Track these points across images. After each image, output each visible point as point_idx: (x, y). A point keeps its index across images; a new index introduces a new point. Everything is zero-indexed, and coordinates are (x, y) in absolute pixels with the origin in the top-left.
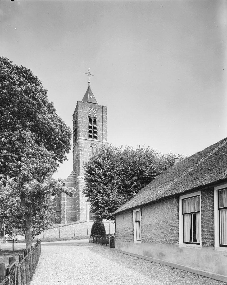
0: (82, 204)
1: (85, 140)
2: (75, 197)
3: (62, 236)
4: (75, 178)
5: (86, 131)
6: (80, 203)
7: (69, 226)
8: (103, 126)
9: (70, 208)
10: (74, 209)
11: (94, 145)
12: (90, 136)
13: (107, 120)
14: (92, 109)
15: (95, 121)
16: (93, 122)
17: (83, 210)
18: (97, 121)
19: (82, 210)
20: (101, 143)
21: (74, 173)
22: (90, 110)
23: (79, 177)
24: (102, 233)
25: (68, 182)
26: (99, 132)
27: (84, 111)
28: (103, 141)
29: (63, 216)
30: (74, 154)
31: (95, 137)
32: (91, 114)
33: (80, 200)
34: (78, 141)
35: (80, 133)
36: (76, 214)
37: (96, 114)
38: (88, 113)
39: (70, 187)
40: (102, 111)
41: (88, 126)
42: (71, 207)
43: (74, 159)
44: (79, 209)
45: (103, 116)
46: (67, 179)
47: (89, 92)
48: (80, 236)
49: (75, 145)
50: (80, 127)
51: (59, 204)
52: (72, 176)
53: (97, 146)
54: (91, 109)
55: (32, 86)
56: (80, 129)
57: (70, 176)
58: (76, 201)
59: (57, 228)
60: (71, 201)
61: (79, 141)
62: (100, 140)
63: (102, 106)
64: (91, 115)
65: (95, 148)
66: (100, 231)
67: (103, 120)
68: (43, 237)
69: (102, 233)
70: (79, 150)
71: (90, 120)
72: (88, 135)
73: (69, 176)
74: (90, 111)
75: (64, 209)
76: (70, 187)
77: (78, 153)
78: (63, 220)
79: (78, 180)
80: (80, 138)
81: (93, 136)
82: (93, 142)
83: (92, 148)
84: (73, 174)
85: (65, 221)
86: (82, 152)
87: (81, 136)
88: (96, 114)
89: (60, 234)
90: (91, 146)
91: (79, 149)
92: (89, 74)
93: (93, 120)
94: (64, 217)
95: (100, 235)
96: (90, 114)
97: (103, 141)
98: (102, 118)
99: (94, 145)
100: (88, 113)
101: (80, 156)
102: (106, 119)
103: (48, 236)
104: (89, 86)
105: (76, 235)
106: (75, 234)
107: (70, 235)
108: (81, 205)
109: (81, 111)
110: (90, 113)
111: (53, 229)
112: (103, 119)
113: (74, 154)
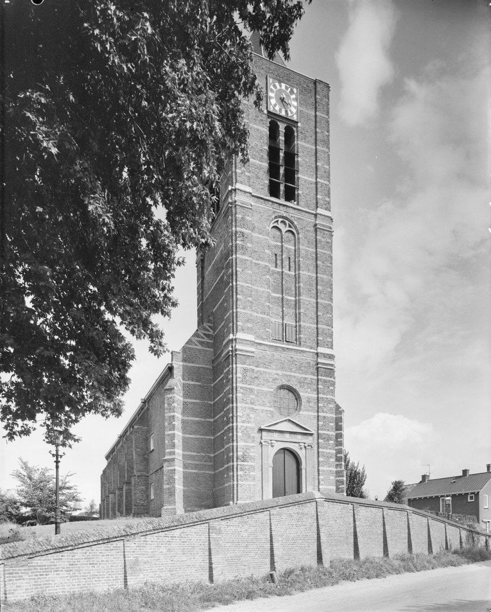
2: (212, 420)
5: (260, 168)
10: (206, 463)
11: (287, 222)
17: (250, 463)
18: (296, 134)
21: (207, 332)
23: (234, 337)
30: (203, 268)
34: (230, 200)
35: (237, 170)
39: (193, 383)
40: (313, 100)
43: (202, 288)
44: (235, 459)
45: (318, 120)
51: (142, 449)
52: (201, 343)
53: (296, 227)
54: (278, 87)
57: (195, 339)
61: (236, 199)
62: (308, 207)
65: (290, 235)
68: (120, 585)
70: (236, 232)
75: (173, 460)
76: (193, 383)
78: (170, 503)
79: (230, 349)
80: (238, 186)
82: (282, 211)
83: (278, 233)
84: (205, 334)
85: (177, 506)
87: (241, 183)
90: (276, 224)
94: (172, 493)
97: (320, 211)
99: (287, 222)
102: (328, 131)
105: (281, 566)
106: (276, 559)
108: (244, 444)
111: (177, 533)
112: (318, 130)
113: (203, 268)
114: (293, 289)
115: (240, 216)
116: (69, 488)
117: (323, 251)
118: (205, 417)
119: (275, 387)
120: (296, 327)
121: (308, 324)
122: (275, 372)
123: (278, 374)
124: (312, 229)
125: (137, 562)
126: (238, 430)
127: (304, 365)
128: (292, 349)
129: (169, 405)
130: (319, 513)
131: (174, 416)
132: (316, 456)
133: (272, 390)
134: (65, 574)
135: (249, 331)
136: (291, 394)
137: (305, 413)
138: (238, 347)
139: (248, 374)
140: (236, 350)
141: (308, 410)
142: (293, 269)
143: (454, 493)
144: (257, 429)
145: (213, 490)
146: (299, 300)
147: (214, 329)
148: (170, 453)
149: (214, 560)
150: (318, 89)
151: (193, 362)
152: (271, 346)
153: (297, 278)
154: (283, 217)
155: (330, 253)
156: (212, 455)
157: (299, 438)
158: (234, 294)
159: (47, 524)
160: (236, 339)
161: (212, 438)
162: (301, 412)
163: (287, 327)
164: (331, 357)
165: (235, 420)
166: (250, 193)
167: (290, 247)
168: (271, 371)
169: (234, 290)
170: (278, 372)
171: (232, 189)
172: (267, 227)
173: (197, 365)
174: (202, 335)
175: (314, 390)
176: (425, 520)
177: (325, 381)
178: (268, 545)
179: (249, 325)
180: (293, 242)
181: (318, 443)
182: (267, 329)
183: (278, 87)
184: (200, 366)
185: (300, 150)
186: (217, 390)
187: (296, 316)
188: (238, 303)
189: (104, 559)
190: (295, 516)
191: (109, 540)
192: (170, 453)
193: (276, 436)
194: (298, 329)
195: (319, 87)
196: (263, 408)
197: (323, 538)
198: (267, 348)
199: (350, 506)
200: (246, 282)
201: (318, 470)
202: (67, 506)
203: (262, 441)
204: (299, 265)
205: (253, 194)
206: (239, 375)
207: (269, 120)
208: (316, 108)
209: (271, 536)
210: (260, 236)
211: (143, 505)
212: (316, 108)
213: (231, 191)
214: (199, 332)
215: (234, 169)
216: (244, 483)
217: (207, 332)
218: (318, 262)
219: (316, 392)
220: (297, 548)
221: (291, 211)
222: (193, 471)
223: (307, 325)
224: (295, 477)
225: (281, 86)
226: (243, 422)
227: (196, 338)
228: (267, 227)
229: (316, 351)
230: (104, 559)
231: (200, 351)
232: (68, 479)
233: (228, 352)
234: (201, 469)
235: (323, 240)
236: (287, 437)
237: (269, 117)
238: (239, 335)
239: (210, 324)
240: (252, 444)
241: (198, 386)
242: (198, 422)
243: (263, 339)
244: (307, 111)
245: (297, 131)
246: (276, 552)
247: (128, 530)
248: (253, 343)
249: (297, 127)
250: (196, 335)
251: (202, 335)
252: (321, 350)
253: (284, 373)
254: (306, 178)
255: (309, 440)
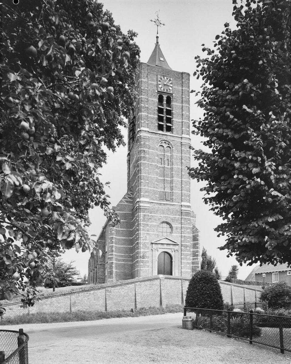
0: (144, 249)
1: (151, 134)
2: (131, 238)
3: (111, 308)
4: (132, 204)
5: (154, 118)
6: (141, 246)
7: (126, 287)
8: (183, 108)
9: (122, 256)
11: (167, 142)
12: (160, 128)
13: (190, 99)
14: (164, 78)
15: (169, 101)
16: (165, 102)
17: (146, 259)
18: (172, 100)
19: (144, 259)
20: (180, 140)
21: (129, 196)
22: (161, 79)
23: (139, 200)
24: (217, 303)
25: (119, 211)
26: (176, 119)
27: (150, 82)
28: (183, 136)
29: (110, 270)
30: (129, 164)
31: (169, 129)
32: (161, 88)
33: (141, 241)
34: (138, 136)
36: (132, 267)
37: (171, 88)
38: (157, 85)
40: (181, 82)
41: (157, 108)
42: (123, 254)
43: (129, 173)
44: (139, 258)
46: (118, 205)
47: (158, 53)
48: (146, 306)
49: (131, 147)
50: (143, 110)
52: (127, 201)
53: (171, 145)
54: (163, 79)
55: (17, 262)
56: (142, 113)
57: (124, 200)
58: (132, 245)
59: (101, 290)
60: (124, 245)
61: (141, 135)
62: (178, 134)
63: (182, 73)
64: (162, 89)
65: (169, 148)
66: (210, 297)
67: (184, 99)
69: (217, 303)
71: (161, 99)
72: (157, 124)
73: (121, 201)
74: (160, 81)
75: (112, 258)
77: (138, 156)
78: (110, 278)
79: (137, 205)
80: (142, 129)
81: (165, 126)
82: (164, 138)
83: (162, 148)
84: (128, 197)
86: (146, 154)
87: (144, 127)
88: (171, 88)
89: (106, 304)
90: (161, 144)
91: (140, 149)
92: (158, 23)
93: (165, 98)
94: (111, 273)
95: (213, 308)
96: (160, 86)
97: (183, 136)
98: (181, 95)
99: (167, 142)
100: (157, 85)
101: (142, 162)
103: (80, 308)
104: (158, 43)
105: (139, 306)
106: (137, 303)
107: (128, 306)
108: (144, 250)
109: (145, 80)
110: (160, 84)
111: (92, 292)
113: (129, 164)
114: (170, 174)
115: (143, 143)
116: (72, 269)
117: (185, 155)
118: (128, 237)
119: (159, 222)
120: (171, 193)
121: (177, 191)
122: (159, 215)
123: (161, 216)
124: (180, 145)
125: (75, 302)
126: (141, 244)
127: (174, 211)
128: (168, 204)
129: (111, 232)
130: (161, 284)
131: (113, 237)
132: (180, 255)
133: (158, 224)
134: (49, 306)
135: (147, 196)
136: (168, 225)
137: (175, 234)
138: (141, 205)
139: (146, 217)
140: (140, 206)
141: (176, 233)
142: (169, 165)
143: (280, 271)
144: (150, 243)
145: (130, 273)
146: (172, 180)
147: (132, 194)
148: (111, 255)
149: (107, 302)
150: (183, 76)
151: (122, 211)
152: (158, 203)
153: (172, 169)
154: (165, 140)
155: (189, 156)
156: (131, 255)
157: (171, 247)
158: (140, 180)
159: (62, 287)
160: (140, 201)
161: (132, 246)
162: (173, 234)
163: (166, 193)
164: (189, 207)
165: (139, 239)
166: (148, 131)
167: (168, 154)
168: (157, 215)
169: (140, 177)
170: (161, 215)
171: (139, 131)
172: (157, 146)
173: (125, 212)
174: (127, 198)
175: (180, 223)
176: (229, 287)
177: (185, 219)
178: (134, 298)
179: (147, 194)
180: (170, 152)
181: (181, 249)
182: (156, 195)
183: (163, 79)
184: (126, 212)
185: (174, 107)
186: (132, 225)
187: (171, 188)
188: (142, 184)
189: (63, 301)
190: (148, 285)
191: (65, 295)
192: (111, 255)
193: (159, 246)
194: (172, 194)
195: (184, 76)
196: (153, 233)
197: (163, 295)
198: (156, 204)
199: (180, 281)
200: (145, 174)
201: (181, 262)
202: (71, 278)
203: (153, 249)
204: (173, 163)
205: (150, 131)
206: (141, 218)
207: (159, 95)
208: (182, 86)
209: (135, 294)
210: (153, 151)
211: (102, 278)
212: (182, 86)
213: (139, 131)
214: (126, 196)
215: (140, 121)
216: (143, 269)
217: (129, 196)
218: (183, 161)
219: (180, 224)
220: (149, 299)
221: (169, 137)
222: (122, 263)
223: (176, 191)
224: (170, 265)
225: (164, 78)
226: (143, 240)
227: (124, 199)
228: (157, 146)
229: (181, 204)
230: (63, 301)
231: (126, 205)
232: (72, 264)
233: (137, 207)
234: (126, 261)
235: (185, 150)
236: (165, 246)
237: (158, 93)
238: (142, 199)
239: (131, 192)
240: (148, 250)
241: (126, 222)
242: (125, 239)
243: (154, 200)
244: (178, 88)
245: (173, 98)
246: (137, 300)
247: (72, 291)
248: (149, 203)
249: (173, 96)
250: (127, 194)
251: (127, 198)
252: (183, 203)
253: (164, 215)
254: (177, 120)
255: (176, 248)
